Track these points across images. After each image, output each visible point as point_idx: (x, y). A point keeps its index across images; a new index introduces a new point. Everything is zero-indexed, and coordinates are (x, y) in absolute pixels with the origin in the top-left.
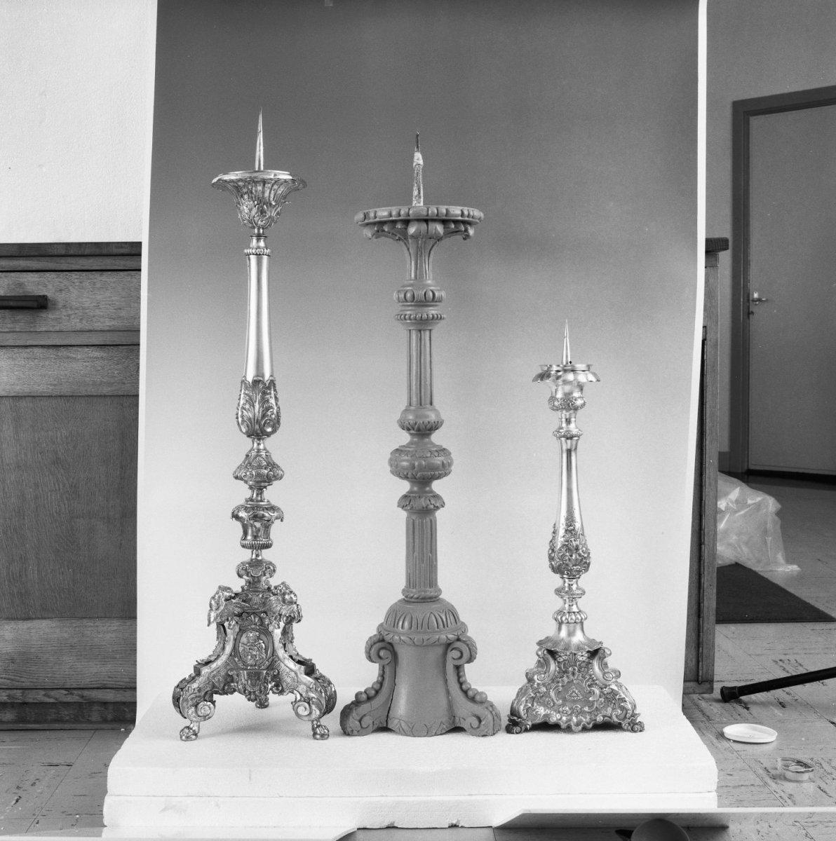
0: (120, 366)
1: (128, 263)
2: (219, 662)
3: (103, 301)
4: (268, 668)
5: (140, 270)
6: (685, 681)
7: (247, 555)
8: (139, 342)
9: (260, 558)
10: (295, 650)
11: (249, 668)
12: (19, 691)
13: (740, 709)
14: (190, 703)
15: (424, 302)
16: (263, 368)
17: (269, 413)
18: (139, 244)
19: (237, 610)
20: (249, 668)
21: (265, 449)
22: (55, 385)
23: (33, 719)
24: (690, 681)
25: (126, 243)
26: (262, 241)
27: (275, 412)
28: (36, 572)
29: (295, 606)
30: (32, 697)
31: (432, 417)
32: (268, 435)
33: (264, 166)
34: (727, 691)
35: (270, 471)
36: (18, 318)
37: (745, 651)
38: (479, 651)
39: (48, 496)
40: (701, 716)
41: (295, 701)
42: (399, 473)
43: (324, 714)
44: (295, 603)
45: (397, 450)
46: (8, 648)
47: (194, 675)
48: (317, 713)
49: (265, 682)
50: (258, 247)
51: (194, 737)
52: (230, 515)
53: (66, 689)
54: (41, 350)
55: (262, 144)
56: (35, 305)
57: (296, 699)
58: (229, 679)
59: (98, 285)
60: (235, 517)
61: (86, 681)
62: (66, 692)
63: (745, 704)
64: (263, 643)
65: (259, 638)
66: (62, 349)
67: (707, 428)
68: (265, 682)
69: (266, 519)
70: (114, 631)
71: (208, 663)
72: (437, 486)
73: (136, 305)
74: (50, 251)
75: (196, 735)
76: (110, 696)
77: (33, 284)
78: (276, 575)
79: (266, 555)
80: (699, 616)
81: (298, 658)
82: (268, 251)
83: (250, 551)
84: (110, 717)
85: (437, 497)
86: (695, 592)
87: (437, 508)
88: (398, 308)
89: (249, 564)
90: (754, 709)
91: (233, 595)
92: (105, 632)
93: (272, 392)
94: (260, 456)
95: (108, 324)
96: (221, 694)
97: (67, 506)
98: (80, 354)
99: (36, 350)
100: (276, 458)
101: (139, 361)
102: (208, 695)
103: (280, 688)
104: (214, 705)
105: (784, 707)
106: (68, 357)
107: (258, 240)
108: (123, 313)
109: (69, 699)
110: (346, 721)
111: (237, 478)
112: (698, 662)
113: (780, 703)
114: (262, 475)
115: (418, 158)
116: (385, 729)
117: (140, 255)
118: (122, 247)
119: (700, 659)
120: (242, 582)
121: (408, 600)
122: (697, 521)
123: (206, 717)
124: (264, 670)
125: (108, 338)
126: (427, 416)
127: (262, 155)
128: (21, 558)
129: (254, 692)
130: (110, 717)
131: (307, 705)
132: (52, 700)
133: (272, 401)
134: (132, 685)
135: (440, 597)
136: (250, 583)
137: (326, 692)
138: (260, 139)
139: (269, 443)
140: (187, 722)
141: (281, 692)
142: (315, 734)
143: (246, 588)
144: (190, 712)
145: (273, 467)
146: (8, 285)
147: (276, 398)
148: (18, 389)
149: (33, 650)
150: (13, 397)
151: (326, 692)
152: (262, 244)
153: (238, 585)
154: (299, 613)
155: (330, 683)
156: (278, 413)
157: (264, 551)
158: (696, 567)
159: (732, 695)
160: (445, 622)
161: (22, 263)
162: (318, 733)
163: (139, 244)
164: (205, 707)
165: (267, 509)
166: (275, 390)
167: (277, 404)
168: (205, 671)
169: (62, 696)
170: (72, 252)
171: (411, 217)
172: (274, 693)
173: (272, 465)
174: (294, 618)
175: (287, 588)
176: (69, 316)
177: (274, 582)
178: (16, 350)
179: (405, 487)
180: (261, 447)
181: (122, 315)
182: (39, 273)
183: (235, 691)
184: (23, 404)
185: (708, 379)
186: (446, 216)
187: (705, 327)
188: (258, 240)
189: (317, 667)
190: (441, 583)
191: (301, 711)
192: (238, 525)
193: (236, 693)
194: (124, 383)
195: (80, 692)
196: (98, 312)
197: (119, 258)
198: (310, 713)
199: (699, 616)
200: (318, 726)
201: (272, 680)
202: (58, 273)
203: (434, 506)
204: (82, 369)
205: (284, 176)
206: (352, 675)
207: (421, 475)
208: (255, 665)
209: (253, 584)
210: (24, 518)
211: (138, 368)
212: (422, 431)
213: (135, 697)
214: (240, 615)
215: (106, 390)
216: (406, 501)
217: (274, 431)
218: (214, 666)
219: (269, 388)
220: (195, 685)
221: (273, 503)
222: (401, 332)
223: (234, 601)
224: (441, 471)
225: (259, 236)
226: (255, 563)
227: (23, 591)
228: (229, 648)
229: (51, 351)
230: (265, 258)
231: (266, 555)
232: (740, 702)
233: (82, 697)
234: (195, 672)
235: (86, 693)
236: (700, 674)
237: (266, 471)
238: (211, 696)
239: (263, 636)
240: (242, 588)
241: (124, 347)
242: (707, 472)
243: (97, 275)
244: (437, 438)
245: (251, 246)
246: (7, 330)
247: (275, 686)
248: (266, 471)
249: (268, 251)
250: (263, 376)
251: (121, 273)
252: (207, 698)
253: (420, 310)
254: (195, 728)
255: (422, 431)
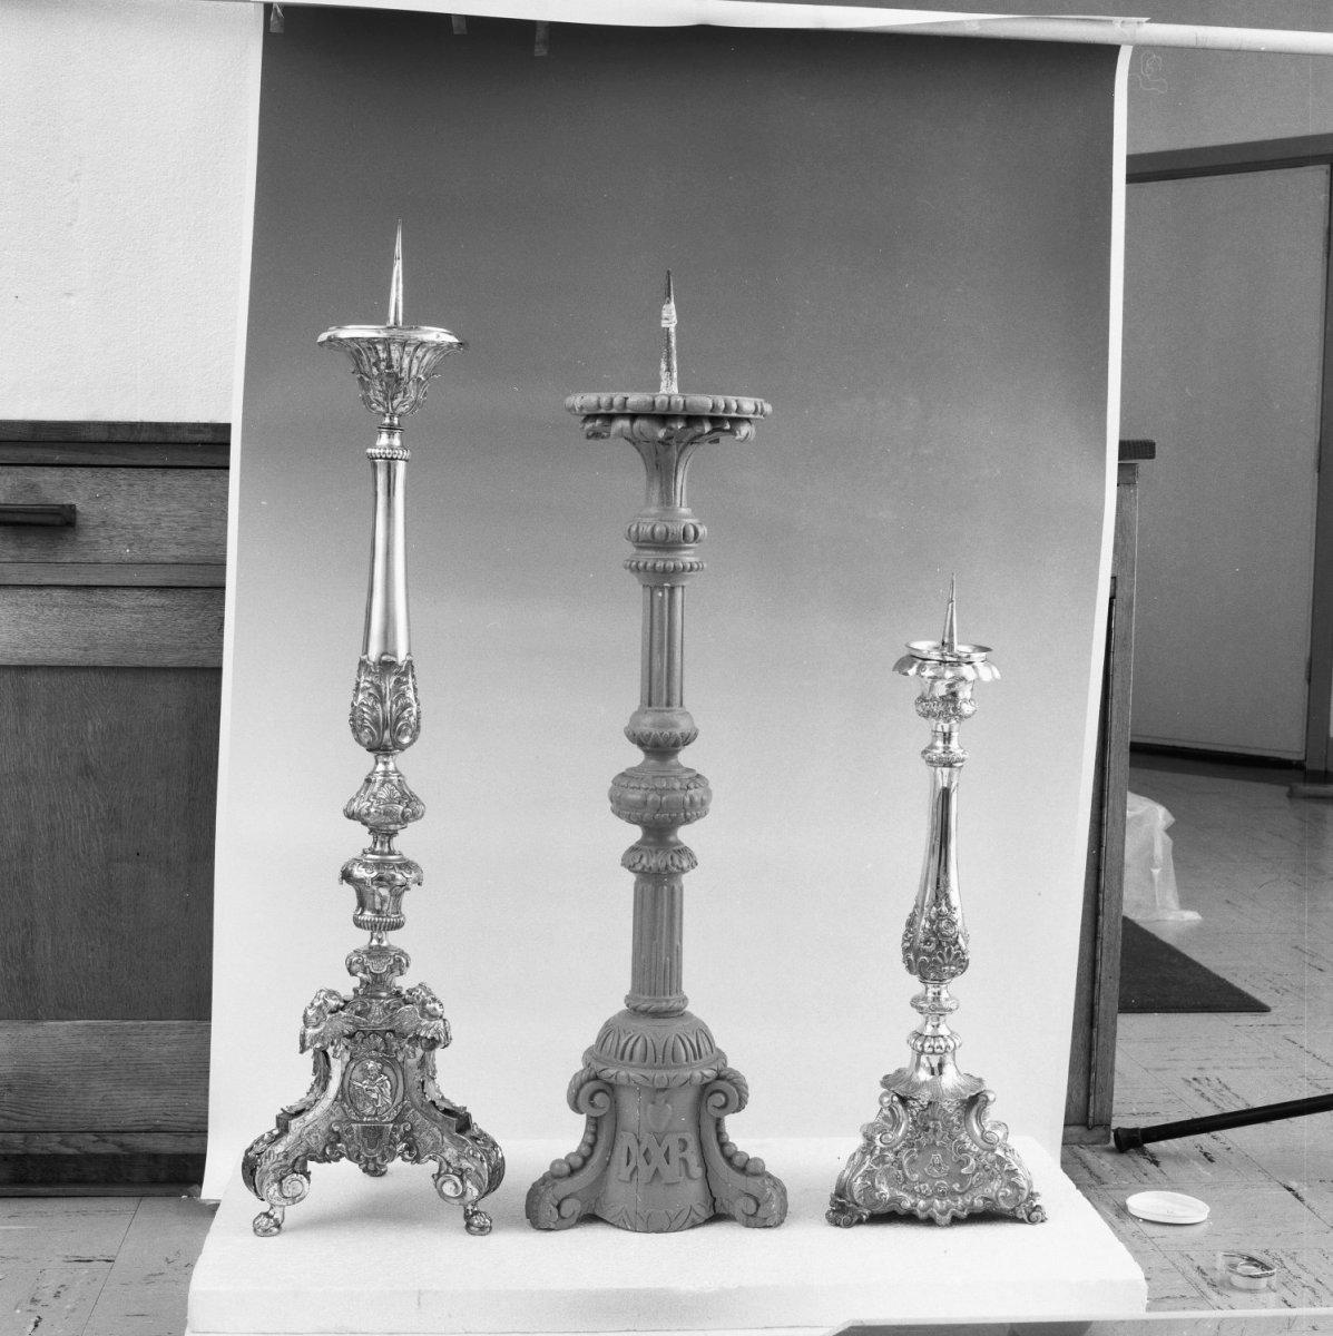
0: (193, 621)
1: (210, 459)
2: (318, 1111)
3: (166, 516)
4: (396, 1121)
5: (228, 468)
6: (1066, 1125)
7: (362, 939)
8: (225, 584)
9: (385, 944)
10: (438, 1091)
11: (365, 1119)
12: (18, 1136)
13: (1144, 1163)
14: (272, 1177)
15: (668, 543)
16: (395, 642)
17: (406, 714)
18: (225, 429)
19: (348, 1029)
20: (365, 1119)
21: (397, 771)
22: (86, 649)
23: (38, 1178)
24: (1070, 1125)
25: (206, 425)
26: (397, 435)
27: (414, 712)
28: (49, 947)
29: (441, 1022)
30: (40, 1145)
31: (683, 726)
32: (402, 748)
33: (404, 315)
34: (1125, 1136)
35: (407, 806)
36: (27, 541)
37: (1161, 1063)
38: (748, 1081)
39: (70, 827)
40: (1087, 1176)
41: (439, 1175)
42: (624, 808)
43: (486, 1194)
44: (441, 1017)
45: (623, 775)
46: (5, 1068)
47: (276, 1132)
48: (473, 1192)
49: (390, 1143)
50: (391, 447)
51: (275, 1230)
52: (339, 874)
53: (95, 1133)
54: (64, 592)
55: (401, 280)
56: (58, 520)
57: (440, 1170)
58: (334, 1139)
59: (159, 491)
60: (347, 876)
61: (128, 1121)
62: (96, 1139)
63: (1152, 1155)
64: (388, 1079)
65: (381, 1072)
66: (99, 592)
67: (1113, 734)
68: (390, 1143)
69: (399, 883)
70: (175, 1041)
71: (299, 1113)
72: (685, 835)
73: (219, 523)
74: (84, 435)
75: (278, 1226)
76: (165, 1145)
77: (54, 487)
78: (409, 972)
79: (392, 939)
80: (1092, 1025)
81: (444, 1105)
82: (406, 454)
83: (369, 932)
84: (163, 1175)
85: (683, 851)
86: (1087, 986)
87: (683, 871)
88: (629, 549)
89: (365, 952)
90: (1166, 1165)
91: (342, 1004)
92: (158, 1039)
93: (410, 680)
94: (390, 781)
95: (173, 552)
96: (319, 1162)
97: (101, 843)
98: (129, 600)
99: (57, 593)
100: (413, 785)
101: (223, 614)
102: (298, 1166)
103: (415, 1152)
104: (309, 1179)
105: (1211, 1160)
106: (108, 605)
107: (391, 435)
108: (198, 536)
109: (102, 1149)
110: (578, 1152)
111: (351, 816)
112: (1088, 1095)
113: (1205, 1154)
114: (386, 819)
115: (670, 316)
116: (591, 1218)
117: (228, 444)
118: (199, 431)
119: (1092, 1091)
120: (355, 982)
121: (635, 1011)
122: (1093, 878)
123: (295, 1199)
124: (388, 1123)
125: (174, 576)
126: (674, 725)
127: (401, 298)
128: (26, 924)
129: (374, 1159)
130: (163, 1175)
131: (457, 1180)
132: (70, 1151)
133: (410, 694)
134: (200, 1127)
135: (686, 1009)
136: (368, 983)
137: (489, 1159)
138: (398, 267)
139: (399, 761)
140: (265, 1207)
141: (417, 1159)
142: (468, 1226)
143: (361, 991)
144: (271, 1192)
145: (411, 801)
146: (13, 487)
147: (415, 690)
148: (25, 655)
149: (42, 1071)
150: (16, 666)
151: (489, 1159)
152: (396, 442)
153: (347, 986)
154: (447, 1034)
155: (495, 1145)
156: (418, 719)
157: (392, 934)
158: (1088, 950)
159: (1132, 1142)
160: (695, 1045)
161: (39, 454)
162: (474, 1223)
163: (227, 427)
164: (294, 1184)
165: (400, 867)
166: (413, 677)
167: (416, 699)
168: (295, 1124)
169: (90, 1145)
170: (118, 437)
171: (614, 411)
172: (404, 1159)
173: (408, 798)
174: (439, 1041)
175: (429, 993)
176: (110, 538)
177: (404, 982)
178: (22, 592)
179: (635, 833)
180: (391, 767)
181: (196, 539)
182: (63, 469)
183: (342, 1155)
184: (32, 679)
185: (1116, 659)
186: (711, 411)
187: (1114, 578)
188: (391, 435)
189: (474, 1120)
190: (687, 989)
191: (448, 1189)
192: (350, 892)
193: (344, 1160)
194: (197, 648)
195: (118, 1138)
196: (157, 534)
197: (201, 448)
198: (464, 1193)
199: (1092, 1025)
200: (475, 1213)
201: (402, 1140)
202: (94, 469)
203: (678, 868)
204: (124, 628)
205: (437, 335)
206: (538, 1134)
207: (659, 817)
208: (376, 1115)
209: (373, 985)
210: (31, 861)
211: (222, 624)
212: (661, 748)
213: (204, 1145)
214: (351, 1036)
215: (171, 659)
216: (631, 860)
217: (414, 738)
218: (309, 1117)
219: (405, 674)
220: (279, 1148)
221: (409, 856)
222: (635, 588)
223: (343, 1014)
224: (690, 811)
225: (391, 429)
226: (377, 952)
227: (28, 977)
228: (334, 1085)
229: (80, 594)
230: (401, 467)
231: (392, 939)
232: (1144, 1153)
233: (121, 1145)
234: (278, 1126)
235: (127, 1139)
236: (1091, 1115)
237: (401, 808)
238: (304, 1164)
239: (387, 1070)
240: (355, 990)
241: (199, 591)
242: (1111, 802)
243: (157, 474)
244: (685, 757)
245: (378, 444)
246: (9, 559)
247: (407, 1148)
248: (401, 808)
249: (406, 454)
250: (395, 655)
251: (197, 472)
252: (297, 1168)
253: (664, 555)
254: (278, 1216)
255: (661, 748)
